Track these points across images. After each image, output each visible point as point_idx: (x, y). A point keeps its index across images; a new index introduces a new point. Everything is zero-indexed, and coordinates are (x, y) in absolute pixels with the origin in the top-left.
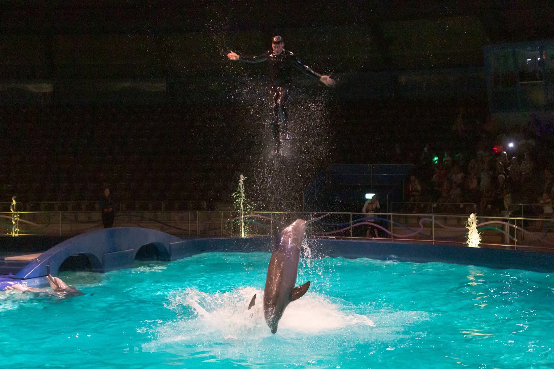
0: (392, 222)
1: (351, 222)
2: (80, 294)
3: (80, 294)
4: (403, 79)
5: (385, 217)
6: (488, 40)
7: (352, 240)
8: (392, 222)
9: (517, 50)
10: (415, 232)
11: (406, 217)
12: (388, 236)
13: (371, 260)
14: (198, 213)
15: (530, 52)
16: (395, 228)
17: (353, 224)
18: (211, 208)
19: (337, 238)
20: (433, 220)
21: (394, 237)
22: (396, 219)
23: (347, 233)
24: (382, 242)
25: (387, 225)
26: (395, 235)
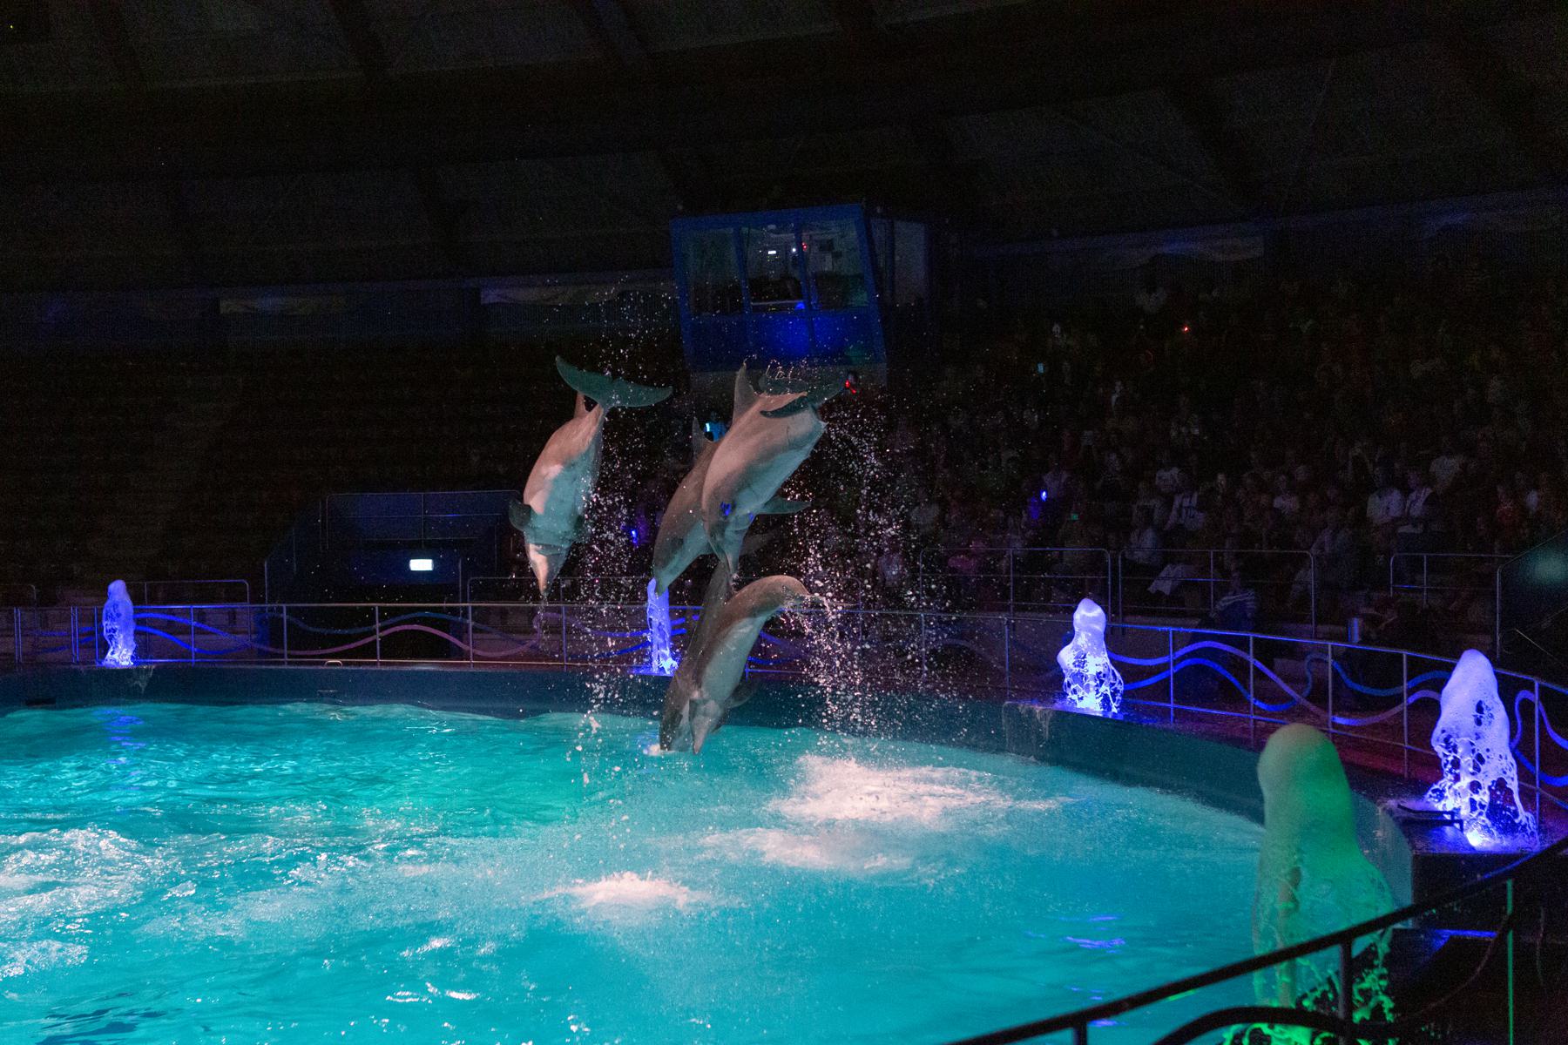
0: (470, 622)
1: (378, 625)
2: (355, 797)
3: (355, 797)
4: (226, 306)
5: (454, 611)
6: (680, 207)
7: (378, 665)
8: (470, 622)
9: (745, 230)
10: (521, 643)
11: (503, 613)
12: (462, 654)
13: (112, 710)
14: (18, 612)
15: (773, 236)
16: (480, 636)
17: (381, 630)
18: (48, 600)
19: (346, 664)
20: (285, 616)
21: (476, 657)
22: (482, 616)
23: (368, 651)
24: (483, 670)
25: (460, 632)
26: (479, 652)
